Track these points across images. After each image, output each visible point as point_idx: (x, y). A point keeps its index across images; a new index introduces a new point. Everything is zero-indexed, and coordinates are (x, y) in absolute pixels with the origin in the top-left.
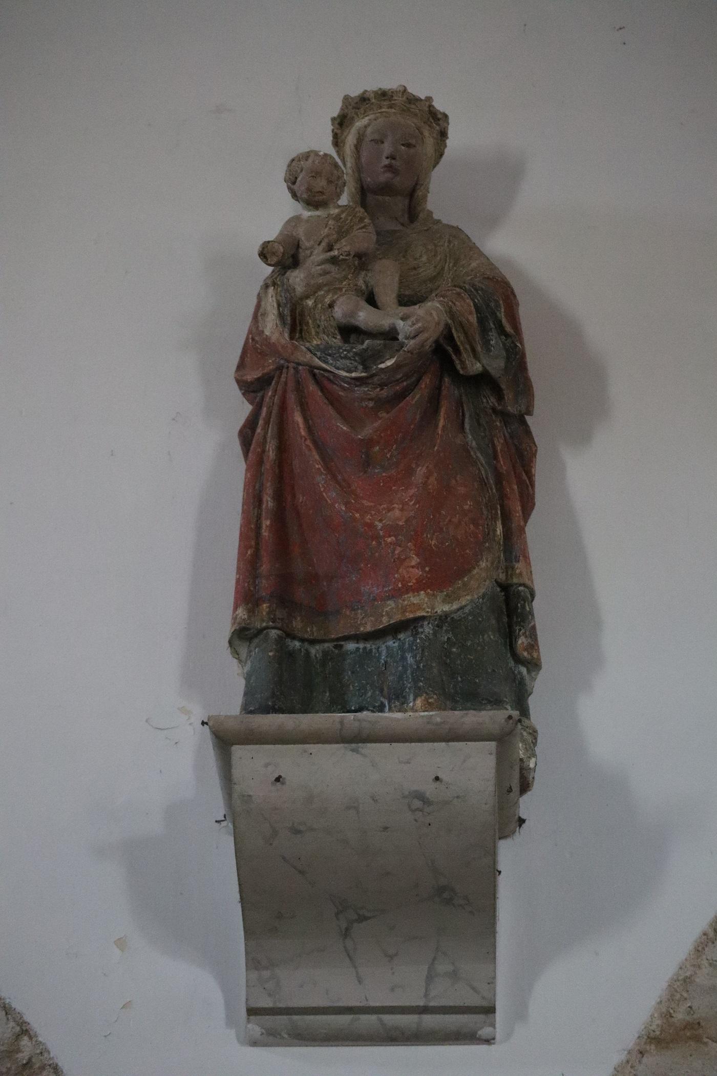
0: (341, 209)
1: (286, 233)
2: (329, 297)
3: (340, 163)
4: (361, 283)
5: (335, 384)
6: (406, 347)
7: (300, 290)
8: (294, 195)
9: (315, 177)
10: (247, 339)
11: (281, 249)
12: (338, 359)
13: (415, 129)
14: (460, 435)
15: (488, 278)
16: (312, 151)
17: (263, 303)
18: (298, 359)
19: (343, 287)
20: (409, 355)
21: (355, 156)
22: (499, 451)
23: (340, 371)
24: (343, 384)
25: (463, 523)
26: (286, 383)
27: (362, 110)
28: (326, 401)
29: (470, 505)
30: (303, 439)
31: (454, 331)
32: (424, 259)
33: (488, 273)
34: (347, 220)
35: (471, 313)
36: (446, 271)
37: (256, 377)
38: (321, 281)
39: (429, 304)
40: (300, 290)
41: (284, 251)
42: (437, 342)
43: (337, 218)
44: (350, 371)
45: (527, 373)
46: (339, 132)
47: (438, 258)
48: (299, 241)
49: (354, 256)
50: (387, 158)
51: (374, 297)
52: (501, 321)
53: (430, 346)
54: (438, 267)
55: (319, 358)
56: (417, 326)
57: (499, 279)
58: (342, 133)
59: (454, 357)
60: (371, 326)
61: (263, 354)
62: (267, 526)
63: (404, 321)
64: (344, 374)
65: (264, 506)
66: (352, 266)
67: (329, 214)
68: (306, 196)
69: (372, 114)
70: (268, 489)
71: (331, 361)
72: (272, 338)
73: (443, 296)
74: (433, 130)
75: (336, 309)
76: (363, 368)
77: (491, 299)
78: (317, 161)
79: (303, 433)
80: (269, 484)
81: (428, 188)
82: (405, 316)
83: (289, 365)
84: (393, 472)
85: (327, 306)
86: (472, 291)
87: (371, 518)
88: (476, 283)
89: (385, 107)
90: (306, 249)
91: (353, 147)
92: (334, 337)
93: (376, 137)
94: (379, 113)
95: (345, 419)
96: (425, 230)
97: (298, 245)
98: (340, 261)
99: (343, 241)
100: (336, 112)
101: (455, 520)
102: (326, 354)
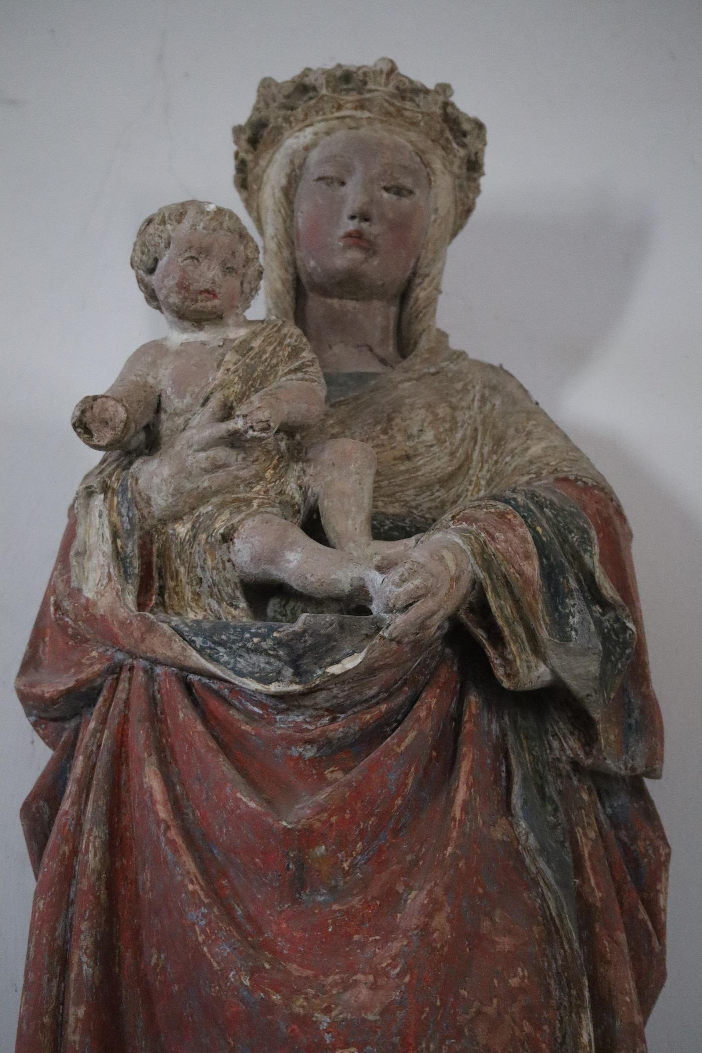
0: (253, 328)
1: (134, 378)
2: (223, 518)
3: (247, 221)
4: (292, 488)
5: (231, 705)
6: (387, 628)
7: (160, 501)
8: (152, 297)
9: (197, 259)
10: (45, 603)
11: (122, 414)
12: (239, 652)
13: (413, 153)
14: (503, 821)
15: (566, 480)
16: (193, 202)
17: (80, 531)
18: (153, 651)
19: (255, 498)
20: (394, 646)
21: (283, 211)
22: (587, 855)
23: (244, 680)
24: (251, 707)
25: (507, 1017)
26: (127, 703)
27: (299, 113)
28: (213, 744)
29: (524, 977)
30: (163, 826)
31: (490, 595)
32: (429, 436)
33: (566, 469)
34: (265, 352)
35: (527, 557)
36: (474, 463)
37: (62, 688)
38: (206, 484)
39: (438, 535)
40: (160, 501)
41: (128, 418)
42: (453, 619)
43: (243, 348)
44: (265, 680)
45: (648, 686)
46: (249, 157)
47: (459, 436)
48: (160, 396)
49: (278, 431)
50: (353, 217)
51: (319, 519)
52: (592, 575)
53: (439, 628)
54: (458, 455)
55: (200, 651)
56: (410, 586)
57: (590, 482)
58: (256, 163)
59: (490, 652)
60: (312, 582)
61: (80, 640)
62: (77, 1020)
63: (383, 573)
64: (252, 685)
65: (73, 976)
66: (274, 453)
67: (225, 340)
68: (177, 301)
69: (319, 122)
70: (82, 937)
71: (226, 658)
72: (99, 603)
73: (466, 519)
74: (451, 156)
75: (238, 544)
76: (294, 674)
77: (571, 527)
78: (202, 224)
79: (163, 812)
80: (84, 926)
81: (439, 284)
82: (385, 562)
83: (135, 662)
84: (356, 902)
85: (219, 537)
86: (531, 510)
87: (305, 1004)
88: (539, 491)
89: (349, 105)
90: (176, 414)
91: (278, 194)
92: (232, 605)
93: (329, 171)
94: (338, 118)
95: (254, 786)
96: (433, 374)
97: (159, 403)
98: (247, 441)
99: (255, 398)
100: (243, 115)
101: (490, 1010)
102: (214, 642)
